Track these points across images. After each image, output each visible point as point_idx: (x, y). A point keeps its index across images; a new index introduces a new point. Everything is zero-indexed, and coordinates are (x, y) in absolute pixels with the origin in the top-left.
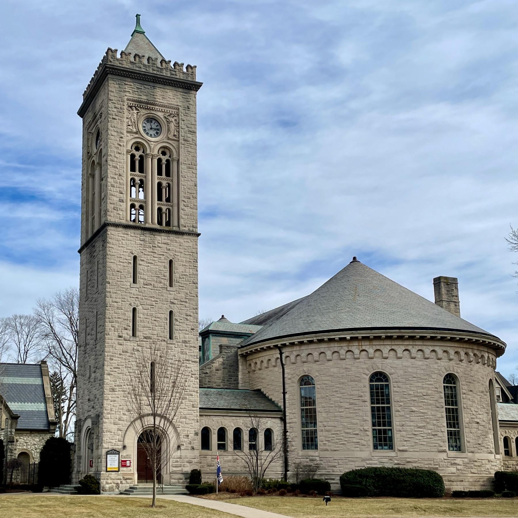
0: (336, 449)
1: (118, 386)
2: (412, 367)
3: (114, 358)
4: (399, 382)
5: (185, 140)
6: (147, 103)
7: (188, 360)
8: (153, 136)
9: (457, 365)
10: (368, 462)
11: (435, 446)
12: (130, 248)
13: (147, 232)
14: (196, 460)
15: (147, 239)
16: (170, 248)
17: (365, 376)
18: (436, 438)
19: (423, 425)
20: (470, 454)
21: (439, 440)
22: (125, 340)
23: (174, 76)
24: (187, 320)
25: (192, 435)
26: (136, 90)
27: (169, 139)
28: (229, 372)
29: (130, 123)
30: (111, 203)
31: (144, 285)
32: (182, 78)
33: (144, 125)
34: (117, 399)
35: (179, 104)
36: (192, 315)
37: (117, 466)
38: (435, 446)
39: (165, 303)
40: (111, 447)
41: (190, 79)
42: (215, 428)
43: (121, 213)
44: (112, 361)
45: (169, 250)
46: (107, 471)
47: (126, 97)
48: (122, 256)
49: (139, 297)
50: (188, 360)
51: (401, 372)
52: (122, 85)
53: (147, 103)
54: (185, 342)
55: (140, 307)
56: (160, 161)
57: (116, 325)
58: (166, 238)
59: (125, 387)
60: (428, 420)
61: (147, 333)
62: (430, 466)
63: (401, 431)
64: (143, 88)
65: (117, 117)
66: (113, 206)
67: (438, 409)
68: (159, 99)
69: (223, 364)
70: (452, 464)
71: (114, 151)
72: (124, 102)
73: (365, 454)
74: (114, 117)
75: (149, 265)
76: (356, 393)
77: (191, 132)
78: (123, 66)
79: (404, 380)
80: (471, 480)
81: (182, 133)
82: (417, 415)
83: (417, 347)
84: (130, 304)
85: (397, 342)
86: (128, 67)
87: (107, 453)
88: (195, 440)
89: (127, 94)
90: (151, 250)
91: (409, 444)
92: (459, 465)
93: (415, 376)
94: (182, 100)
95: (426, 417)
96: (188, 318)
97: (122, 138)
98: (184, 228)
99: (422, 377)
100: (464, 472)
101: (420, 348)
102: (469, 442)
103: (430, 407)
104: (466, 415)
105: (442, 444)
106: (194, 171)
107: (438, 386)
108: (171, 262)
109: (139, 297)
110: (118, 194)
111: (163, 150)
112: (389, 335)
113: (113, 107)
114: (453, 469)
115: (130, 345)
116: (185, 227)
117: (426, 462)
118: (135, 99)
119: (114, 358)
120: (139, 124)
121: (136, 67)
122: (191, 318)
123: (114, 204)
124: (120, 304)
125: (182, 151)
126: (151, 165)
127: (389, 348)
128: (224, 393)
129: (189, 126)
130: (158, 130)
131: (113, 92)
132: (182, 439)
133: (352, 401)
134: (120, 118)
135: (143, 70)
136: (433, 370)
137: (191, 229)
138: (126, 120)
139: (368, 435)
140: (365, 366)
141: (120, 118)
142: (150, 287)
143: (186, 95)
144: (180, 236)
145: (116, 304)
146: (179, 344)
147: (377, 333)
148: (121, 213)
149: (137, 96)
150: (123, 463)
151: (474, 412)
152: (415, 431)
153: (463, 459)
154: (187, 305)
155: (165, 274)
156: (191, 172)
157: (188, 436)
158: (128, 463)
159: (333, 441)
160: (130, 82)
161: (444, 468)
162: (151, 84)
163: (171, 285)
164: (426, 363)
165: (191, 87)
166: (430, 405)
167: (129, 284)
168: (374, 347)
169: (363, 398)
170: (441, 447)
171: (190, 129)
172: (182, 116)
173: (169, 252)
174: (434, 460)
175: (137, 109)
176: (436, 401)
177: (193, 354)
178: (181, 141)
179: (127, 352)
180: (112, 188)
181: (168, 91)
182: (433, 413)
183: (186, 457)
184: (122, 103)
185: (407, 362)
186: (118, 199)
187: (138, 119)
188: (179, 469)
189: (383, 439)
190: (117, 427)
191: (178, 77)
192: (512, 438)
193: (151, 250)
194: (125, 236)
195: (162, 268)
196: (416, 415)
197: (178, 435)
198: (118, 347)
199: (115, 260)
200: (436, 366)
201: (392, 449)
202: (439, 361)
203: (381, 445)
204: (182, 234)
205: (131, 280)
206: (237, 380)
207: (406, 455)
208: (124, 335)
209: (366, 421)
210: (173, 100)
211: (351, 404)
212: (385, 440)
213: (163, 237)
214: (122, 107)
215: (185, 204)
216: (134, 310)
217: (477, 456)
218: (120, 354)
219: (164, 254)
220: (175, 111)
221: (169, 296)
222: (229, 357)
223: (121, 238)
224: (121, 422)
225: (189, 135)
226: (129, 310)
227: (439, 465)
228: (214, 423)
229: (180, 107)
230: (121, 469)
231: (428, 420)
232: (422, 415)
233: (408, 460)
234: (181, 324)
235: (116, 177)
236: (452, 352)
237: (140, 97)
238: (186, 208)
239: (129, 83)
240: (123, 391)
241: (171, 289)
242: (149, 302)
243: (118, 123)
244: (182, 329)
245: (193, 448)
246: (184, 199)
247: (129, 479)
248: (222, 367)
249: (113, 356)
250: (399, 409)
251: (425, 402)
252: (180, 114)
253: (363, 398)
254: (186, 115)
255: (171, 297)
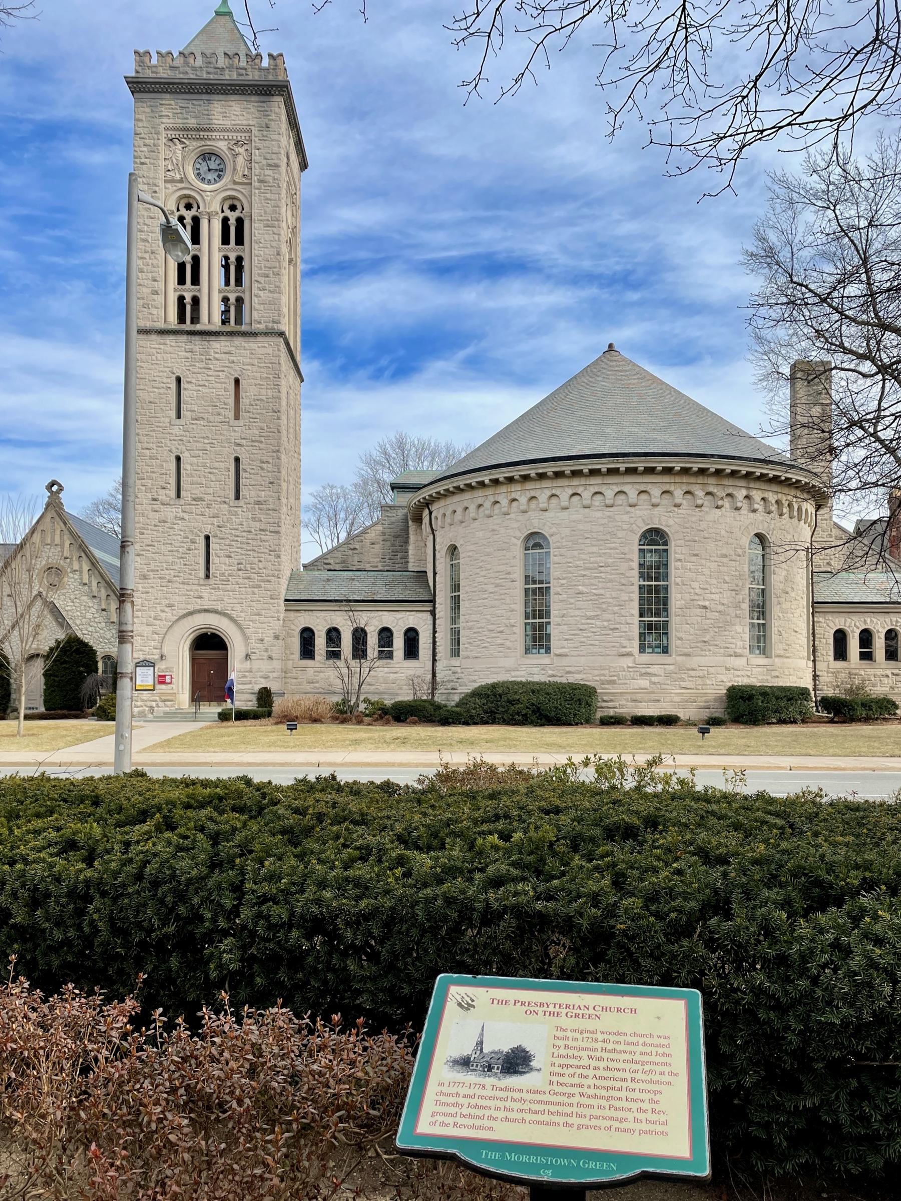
0: (477, 655)
1: (153, 571)
2: (586, 522)
3: (145, 532)
4: (563, 547)
5: (260, 181)
6: (199, 130)
7: (263, 530)
8: (213, 181)
9: (667, 514)
10: (513, 674)
11: (614, 647)
12: (170, 365)
13: (197, 338)
14: (275, 675)
15: (197, 348)
16: (235, 359)
17: (515, 541)
18: (615, 634)
19: (595, 613)
20: (679, 659)
21: (621, 637)
22: (163, 504)
23: (243, 78)
24: (262, 469)
25: (268, 639)
26: (179, 111)
27: (235, 183)
28: (393, 545)
29: (170, 168)
30: (138, 298)
31: (193, 419)
32: (257, 78)
33: (198, 166)
34: (150, 590)
35: (251, 123)
36: (271, 461)
37: (151, 683)
38: (614, 647)
39: (226, 445)
40: (142, 657)
41: (271, 78)
42: (320, 628)
43: (154, 312)
44: (142, 536)
45: (233, 362)
46: (136, 690)
47: (163, 126)
48: (157, 379)
49: (184, 438)
50: (263, 530)
51: (567, 531)
52: (157, 106)
53: (199, 130)
54: (258, 503)
55: (187, 454)
56: (225, 221)
57: (149, 483)
58: (228, 344)
59: (162, 572)
60: (604, 606)
61: (198, 492)
62: (602, 678)
63: (559, 625)
64: (190, 106)
65: (147, 161)
66: (141, 302)
67: (623, 587)
68: (218, 120)
69: (384, 534)
70: (641, 675)
71: (143, 216)
72: (158, 133)
73: (509, 663)
74: (142, 161)
75: (200, 388)
76: (502, 568)
77: (270, 165)
78: (158, 76)
79: (570, 543)
80: (677, 699)
81: (256, 170)
82: (588, 598)
83: (637, 487)
84: (170, 451)
85: (538, 485)
86: (165, 76)
87: (137, 665)
88: (274, 646)
89: (165, 120)
90: (203, 365)
91: (571, 645)
92: (655, 675)
93: (587, 535)
94: (257, 115)
95: (601, 601)
96: (264, 465)
97: (155, 192)
98: (258, 326)
99: (599, 538)
100: (665, 687)
101: (597, 489)
102: (681, 639)
103: (609, 585)
104: (679, 596)
105: (626, 643)
106: (275, 230)
107: (626, 550)
108: (237, 381)
109: (184, 438)
110: (150, 282)
111: (230, 202)
112: (541, 471)
113: (142, 144)
114: (644, 683)
115: (170, 513)
116: (260, 323)
117: (596, 672)
118: (171, 125)
119: (145, 532)
120: (186, 166)
121: (180, 73)
122: (270, 466)
123: (143, 299)
124: (154, 451)
125: (255, 199)
126: (211, 231)
127: (548, 493)
128: (362, 577)
129: (268, 156)
130: (221, 170)
131: (142, 120)
132: (254, 644)
133: (498, 581)
134: (152, 161)
135: (192, 76)
136: (620, 524)
137: (270, 325)
138: (162, 163)
139: (515, 633)
140: (515, 525)
141: (152, 161)
142: (202, 423)
143: (264, 105)
144: (252, 339)
145: (148, 451)
146: (249, 506)
147: (524, 470)
148: (154, 312)
149: (180, 121)
150: (161, 679)
151: (698, 591)
152: (583, 624)
153: (666, 666)
154: (262, 446)
155: (226, 401)
156: (271, 232)
157: (262, 640)
158: (168, 679)
159: (475, 644)
160: (169, 100)
161: (628, 682)
162: (205, 97)
163: (237, 417)
164: (608, 514)
165: (270, 92)
166: (611, 581)
167: (167, 420)
168: (527, 492)
169: (511, 576)
170: (625, 647)
171: (270, 162)
172: (256, 142)
173: (232, 365)
174: (609, 669)
175: (182, 143)
176: (622, 574)
177: (271, 521)
178: (256, 184)
179: (165, 522)
180: (140, 274)
181: (233, 103)
182: (614, 594)
183: (259, 670)
184: (155, 136)
185: (576, 514)
186: (149, 291)
187: (184, 157)
188: (249, 686)
189: (539, 639)
190: (151, 628)
191: (250, 78)
192: (878, 632)
193: (203, 365)
194: (162, 346)
195: (222, 392)
196: (585, 599)
197: (246, 638)
198: (152, 515)
199: (146, 385)
200: (626, 518)
201: (667, 652)
202: (632, 509)
203: (534, 647)
204: (254, 334)
205: (173, 414)
206: (405, 558)
207: (565, 661)
208: (160, 498)
209: (513, 610)
210: (241, 118)
211: (497, 586)
212: (541, 638)
213: (223, 343)
214: (156, 142)
215: (260, 286)
216: (178, 459)
217: (695, 661)
218: (155, 526)
219: (225, 369)
220: (246, 134)
221: (232, 434)
222: (392, 523)
223: (154, 351)
224: (157, 622)
225: (267, 172)
226: (168, 459)
227: (618, 676)
228: (320, 622)
229: (253, 128)
230: (158, 686)
231: (604, 606)
232: (596, 597)
233: (568, 669)
234: (252, 476)
235: (147, 256)
236: (678, 493)
237: (185, 121)
238: (261, 293)
239: (167, 102)
240: (160, 578)
241: (237, 423)
242: (199, 445)
243: (150, 169)
244: (253, 483)
245: (270, 658)
246: (259, 279)
247: (169, 701)
248: (381, 538)
249: (144, 528)
250: (559, 589)
251: (601, 577)
252: (253, 138)
253: (511, 576)
254: (263, 139)
255: (234, 436)
